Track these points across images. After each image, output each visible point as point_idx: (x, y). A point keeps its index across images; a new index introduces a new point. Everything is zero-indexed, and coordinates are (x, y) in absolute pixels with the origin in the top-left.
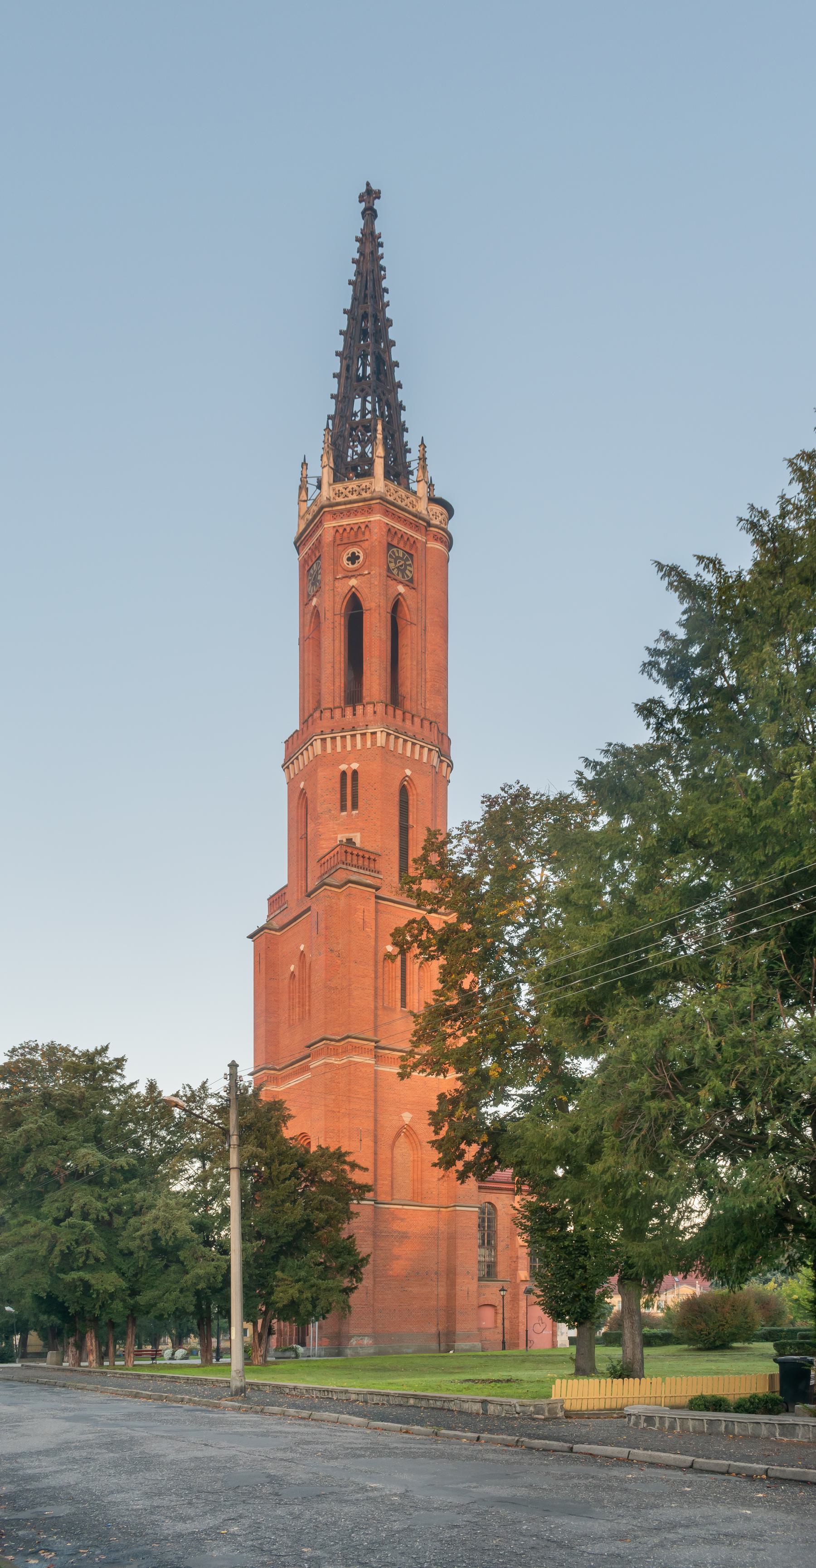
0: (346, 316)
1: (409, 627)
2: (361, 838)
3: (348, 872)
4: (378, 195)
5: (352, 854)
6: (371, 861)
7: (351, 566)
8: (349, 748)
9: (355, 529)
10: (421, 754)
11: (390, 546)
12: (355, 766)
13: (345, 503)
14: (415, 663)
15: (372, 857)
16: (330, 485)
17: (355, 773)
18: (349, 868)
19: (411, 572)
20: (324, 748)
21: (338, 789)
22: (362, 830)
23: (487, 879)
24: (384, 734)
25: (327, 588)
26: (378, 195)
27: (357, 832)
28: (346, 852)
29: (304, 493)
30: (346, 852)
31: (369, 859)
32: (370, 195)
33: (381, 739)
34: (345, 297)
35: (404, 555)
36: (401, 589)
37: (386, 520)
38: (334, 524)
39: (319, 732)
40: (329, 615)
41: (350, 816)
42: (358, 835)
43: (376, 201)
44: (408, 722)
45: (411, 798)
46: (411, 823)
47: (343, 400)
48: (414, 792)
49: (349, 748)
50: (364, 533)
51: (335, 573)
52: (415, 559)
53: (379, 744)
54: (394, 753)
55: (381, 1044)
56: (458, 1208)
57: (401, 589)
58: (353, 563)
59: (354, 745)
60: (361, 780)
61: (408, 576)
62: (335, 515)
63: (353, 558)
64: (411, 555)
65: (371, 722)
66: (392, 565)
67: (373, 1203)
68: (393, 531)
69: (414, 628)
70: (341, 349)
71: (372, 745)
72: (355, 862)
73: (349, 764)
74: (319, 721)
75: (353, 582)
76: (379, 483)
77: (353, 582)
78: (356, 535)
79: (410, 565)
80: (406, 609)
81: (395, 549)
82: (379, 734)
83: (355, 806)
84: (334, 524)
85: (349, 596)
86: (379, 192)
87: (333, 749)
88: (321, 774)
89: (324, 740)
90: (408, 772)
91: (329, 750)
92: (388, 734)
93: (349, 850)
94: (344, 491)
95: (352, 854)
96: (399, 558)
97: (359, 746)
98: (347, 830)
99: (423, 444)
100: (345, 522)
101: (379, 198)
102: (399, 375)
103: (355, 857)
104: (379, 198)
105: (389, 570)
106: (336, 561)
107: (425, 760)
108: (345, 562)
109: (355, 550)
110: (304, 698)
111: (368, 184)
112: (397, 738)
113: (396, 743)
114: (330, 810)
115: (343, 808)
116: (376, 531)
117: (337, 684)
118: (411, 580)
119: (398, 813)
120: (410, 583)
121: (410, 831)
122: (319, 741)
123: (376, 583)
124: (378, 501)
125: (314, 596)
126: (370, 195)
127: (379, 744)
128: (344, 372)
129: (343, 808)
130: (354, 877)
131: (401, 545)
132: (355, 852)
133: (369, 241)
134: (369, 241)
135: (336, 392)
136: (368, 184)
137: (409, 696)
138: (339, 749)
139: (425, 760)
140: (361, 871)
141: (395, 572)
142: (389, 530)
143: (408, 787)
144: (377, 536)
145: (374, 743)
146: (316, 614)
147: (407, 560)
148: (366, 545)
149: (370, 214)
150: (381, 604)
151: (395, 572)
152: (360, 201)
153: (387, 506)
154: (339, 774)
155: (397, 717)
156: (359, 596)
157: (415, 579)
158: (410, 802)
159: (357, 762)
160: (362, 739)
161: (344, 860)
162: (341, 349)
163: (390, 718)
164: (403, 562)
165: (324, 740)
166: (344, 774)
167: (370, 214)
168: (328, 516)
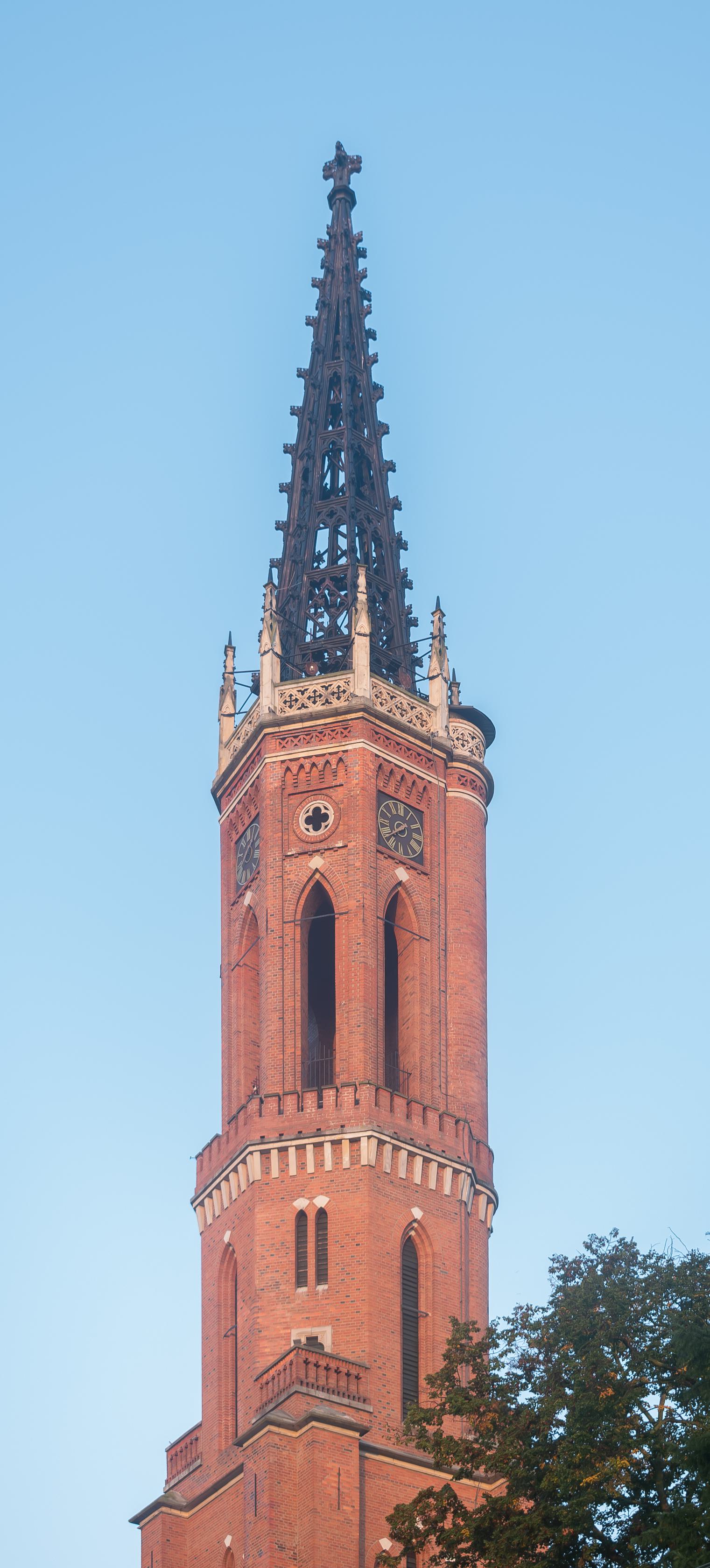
1: (416, 944)
2: (334, 1335)
3: (309, 1399)
4: (356, 165)
5: (317, 1365)
6: (353, 1380)
7: (312, 833)
8: (310, 1169)
9: (320, 767)
10: (440, 1179)
11: (381, 796)
12: (321, 1201)
13: (301, 719)
14: (427, 1011)
15: (354, 1372)
16: (275, 686)
17: (322, 1213)
18: (313, 1392)
19: (419, 843)
21: (292, 1245)
22: (334, 1321)
24: (374, 1142)
25: (271, 873)
26: (356, 165)
27: (326, 1324)
28: (306, 1362)
29: (228, 701)
30: (306, 1362)
31: (348, 1375)
32: (343, 165)
35: (406, 812)
36: (402, 874)
37: (374, 749)
38: (283, 755)
39: (257, 1138)
40: (274, 924)
41: (313, 1294)
42: (328, 1330)
43: (354, 176)
44: (417, 1120)
45: (422, 1261)
46: (422, 1308)
47: (298, 531)
48: (429, 1250)
49: (310, 1169)
50: (335, 773)
51: (284, 845)
52: (427, 819)
53: (364, 1161)
54: (391, 1178)
57: (402, 874)
58: (317, 828)
59: (319, 1164)
60: (333, 1228)
61: (414, 852)
62: (283, 740)
64: (420, 813)
65: (349, 1119)
66: (385, 831)
68: (387, 768)
69: (427, 946)
71: (352, 1164)
72: (322, 1382)
73: (311, 1199)
74: (256, 1119)
76: (361, 681)
77: (317, 862)
78: (320, 777)
79: (417, 831)
80: (411, 910)
82: (364, 1142)
83: (322, 1276)
84: (283, 755)
85: (309, 887)
86: (359, 160)
87: (282, 1171)
88: (261, 1216)
89: (265, 1153)
90: (417, 1213)
91: (275, 1172)
92: (381, 1143)
93: (312, 1359)
94: (299, 696)
95: (317, 1365)
96: (398, 817)
97: (328, 1165)
98: (309, 1321)
100: (301, 753)
102: (395, 485)
103: (322, 1372)
104: (358, 170)
105: (380, 840)
106: (286, 824)
107: (447, 1190)
108: (303, 825)
109: (320, 803)
110: (230, 1075)
111: (339, 146)
112: (396, 1149)
113: (394, 1159)
114: (277, 1284)
115: (301, 1280)
116: (357, 768)
117: (289, 1050)
118: (420, 859)
119: (398, 1290)
120: (417, 864)
121: (422, 1323)
122: (257, 1155)
123: (358, 864)
124: (360, 714)
126: (343, 165)
127: (364, 1161)
129: (301, 1280)
131: (402, 795)
132: (323, 1363)
133: (342, 252)
134: (342, 252)
136: (339, 146)
137: (417, 1073)
138: (293, 1170)
139: (447, 1190)
140: (334, 1398)
142: (380, 766)
144: (358, 779)
145: (355, 1158)
146: (252, 919)
147: (412, 821)
148: (338, 794)
149: (342, 199)
150: (367, 903)
153: (377, 724)
154: (293, 1217)
155: (397, 1110)
156: (327, 887)
157: (427, 856)
158: (422, 1269)
159: (327, 1194)
160: (334, 1151)
161: (303, 1377)
163: (384, 1112)
165: (265, 1153)
166: (302, 1215)
167: (342, 199)
168: (272, 743)
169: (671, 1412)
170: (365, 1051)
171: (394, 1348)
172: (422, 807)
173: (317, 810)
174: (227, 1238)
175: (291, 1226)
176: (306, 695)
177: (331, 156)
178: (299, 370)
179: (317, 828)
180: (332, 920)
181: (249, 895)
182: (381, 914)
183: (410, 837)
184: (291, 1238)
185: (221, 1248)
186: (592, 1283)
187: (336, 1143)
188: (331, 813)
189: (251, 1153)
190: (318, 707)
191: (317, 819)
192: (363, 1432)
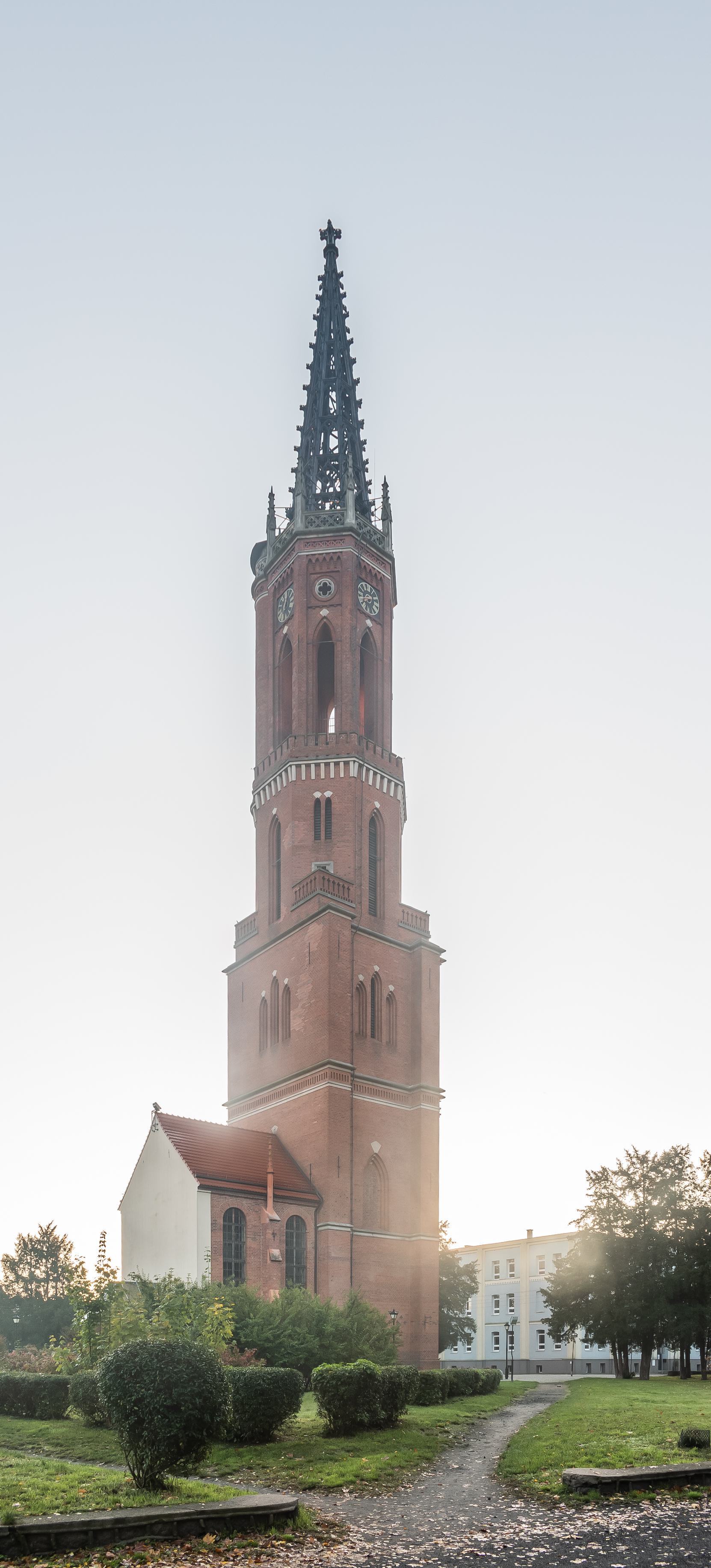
0: (306, 392)
4: (338, 234)
12: (328, 794)
17: (329, 801)
20: (299, 774)
23: (270, 1147)
24: (357, 765)
30: (324, 878)
32: (330, 234)
34: (316, 288)
43: (337, 240)
55: (357, 1073)
56: (329, 1227)
57: (369, 623)
58: (325, 594)
60: (335, 806)
63: (325, 589)
67: (349, 1229)
70: (308, 383)
77: (324, 612)
81: (364, 583)
82: (351, 764)
83: (328, 835)
85: (321, 625)
86: (340, 231)
99: (385, 485)
101: (340, 237)
102: (361, 414)
104: (340, 237)
111: (329, 222)
122: (294, 768)
125: (285, 624)
128: (302, 486)
130: (332, 903)
135: (302, 425)
136: (329, 222)
141: (364, 606)
146: (287, 642)
149: (331, 253)
151: (364, 606)
152: (322, 239)
154: (313, 803)
162: (308, 383)
164: (370, 598)
165: (298, 767)
166: (318, 801)
167: (331, 253)
169: (227, 1389)
173: (325, 584)
174: (274, 811)
176: (320, 520)
177: (325, 227)
178: (310, 344)
179: (325, 594)
180: (333, 645)
181: (286, 628)
183: (373, 604)
185: (270, 819)
186: (118, 1368)
188: (333, 586)
189: (291, 766)
190: (327, 527)
192: (353, 917)
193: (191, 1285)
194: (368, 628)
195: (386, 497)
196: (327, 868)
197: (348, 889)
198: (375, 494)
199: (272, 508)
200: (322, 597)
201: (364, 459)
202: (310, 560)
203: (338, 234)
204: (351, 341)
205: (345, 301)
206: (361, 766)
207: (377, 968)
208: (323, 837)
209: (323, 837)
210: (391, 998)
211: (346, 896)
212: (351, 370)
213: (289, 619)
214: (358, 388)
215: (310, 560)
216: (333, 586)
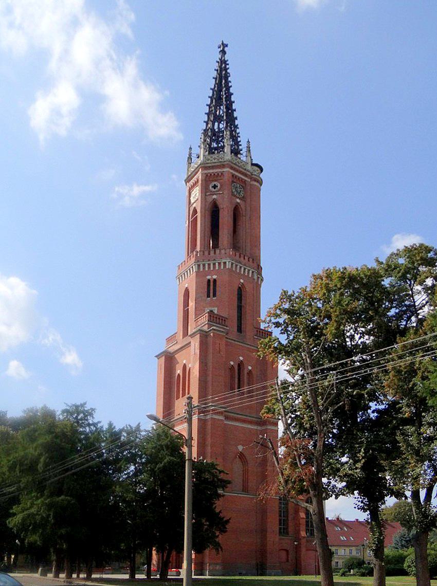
12: (215, 277)
17: (215, 281)
26: (227, 46)
33: (228, 266)
36: (238, 201)
42: (216, 309)
50: (220, 177)
57: (238, 201)
63: (215, 187)
75: (215, 197)
77: (215, 197)
82: (227, 263)
83: (214, 295)
97: (217, 268)
98: (210, 306)
109: (215, 183)
127: (227, 267)
129: (208, 296)
133: (222, 95)
134: (222, 95)
138: (207, 269)
141: (235, 193)
143: (242, 288)
144: (227, 177)
166: (209, 281)
167: (223, 52)
170: (228, 241)
171: (235, 313)
172: (244, 185)
175: (206, 283)
179: (215, 188)
180: (219, 210)
182: (233, 209)
184: (206, 286)
187: (219, 264)
191: (215, 187)
193: (156, 435)
194: (238, 203)
195: (248, 147)
196: (213, 311)
197: (225, 321)
198: (243, 146)
199: (190, 155)
200: (213, 190)
201: (235, 116)
202: (207, 175)
203: (227, 46)
204: (231, 86)
205: (237, 122)
206: (232, 264)
207: (241, 358)
208: (211, 294)
209: (211, 294)
210: (250, 372)
211: (223, 323)
212: (231, 98)
213: (196, 201)
214: (232, 96)
215: (207, 175)
216: (211, 188)
